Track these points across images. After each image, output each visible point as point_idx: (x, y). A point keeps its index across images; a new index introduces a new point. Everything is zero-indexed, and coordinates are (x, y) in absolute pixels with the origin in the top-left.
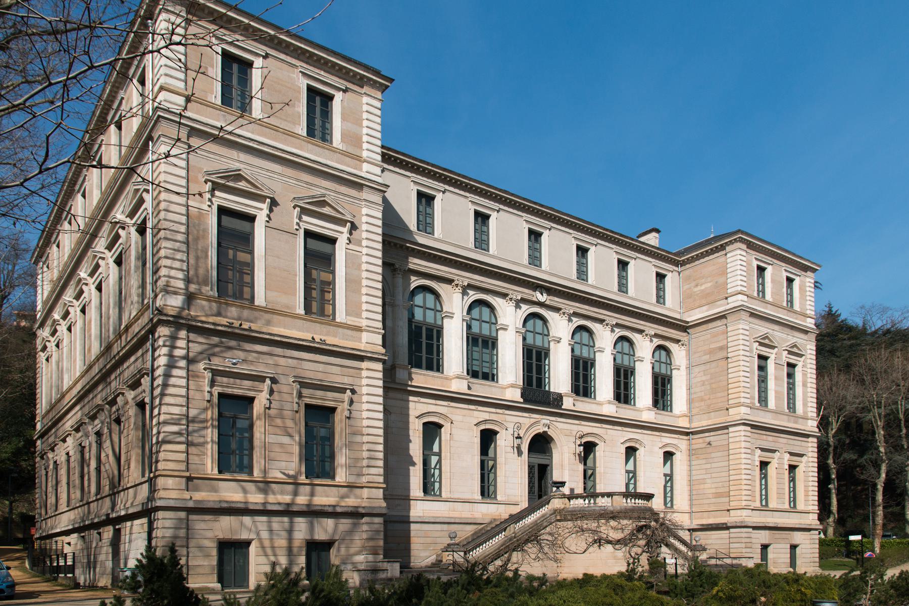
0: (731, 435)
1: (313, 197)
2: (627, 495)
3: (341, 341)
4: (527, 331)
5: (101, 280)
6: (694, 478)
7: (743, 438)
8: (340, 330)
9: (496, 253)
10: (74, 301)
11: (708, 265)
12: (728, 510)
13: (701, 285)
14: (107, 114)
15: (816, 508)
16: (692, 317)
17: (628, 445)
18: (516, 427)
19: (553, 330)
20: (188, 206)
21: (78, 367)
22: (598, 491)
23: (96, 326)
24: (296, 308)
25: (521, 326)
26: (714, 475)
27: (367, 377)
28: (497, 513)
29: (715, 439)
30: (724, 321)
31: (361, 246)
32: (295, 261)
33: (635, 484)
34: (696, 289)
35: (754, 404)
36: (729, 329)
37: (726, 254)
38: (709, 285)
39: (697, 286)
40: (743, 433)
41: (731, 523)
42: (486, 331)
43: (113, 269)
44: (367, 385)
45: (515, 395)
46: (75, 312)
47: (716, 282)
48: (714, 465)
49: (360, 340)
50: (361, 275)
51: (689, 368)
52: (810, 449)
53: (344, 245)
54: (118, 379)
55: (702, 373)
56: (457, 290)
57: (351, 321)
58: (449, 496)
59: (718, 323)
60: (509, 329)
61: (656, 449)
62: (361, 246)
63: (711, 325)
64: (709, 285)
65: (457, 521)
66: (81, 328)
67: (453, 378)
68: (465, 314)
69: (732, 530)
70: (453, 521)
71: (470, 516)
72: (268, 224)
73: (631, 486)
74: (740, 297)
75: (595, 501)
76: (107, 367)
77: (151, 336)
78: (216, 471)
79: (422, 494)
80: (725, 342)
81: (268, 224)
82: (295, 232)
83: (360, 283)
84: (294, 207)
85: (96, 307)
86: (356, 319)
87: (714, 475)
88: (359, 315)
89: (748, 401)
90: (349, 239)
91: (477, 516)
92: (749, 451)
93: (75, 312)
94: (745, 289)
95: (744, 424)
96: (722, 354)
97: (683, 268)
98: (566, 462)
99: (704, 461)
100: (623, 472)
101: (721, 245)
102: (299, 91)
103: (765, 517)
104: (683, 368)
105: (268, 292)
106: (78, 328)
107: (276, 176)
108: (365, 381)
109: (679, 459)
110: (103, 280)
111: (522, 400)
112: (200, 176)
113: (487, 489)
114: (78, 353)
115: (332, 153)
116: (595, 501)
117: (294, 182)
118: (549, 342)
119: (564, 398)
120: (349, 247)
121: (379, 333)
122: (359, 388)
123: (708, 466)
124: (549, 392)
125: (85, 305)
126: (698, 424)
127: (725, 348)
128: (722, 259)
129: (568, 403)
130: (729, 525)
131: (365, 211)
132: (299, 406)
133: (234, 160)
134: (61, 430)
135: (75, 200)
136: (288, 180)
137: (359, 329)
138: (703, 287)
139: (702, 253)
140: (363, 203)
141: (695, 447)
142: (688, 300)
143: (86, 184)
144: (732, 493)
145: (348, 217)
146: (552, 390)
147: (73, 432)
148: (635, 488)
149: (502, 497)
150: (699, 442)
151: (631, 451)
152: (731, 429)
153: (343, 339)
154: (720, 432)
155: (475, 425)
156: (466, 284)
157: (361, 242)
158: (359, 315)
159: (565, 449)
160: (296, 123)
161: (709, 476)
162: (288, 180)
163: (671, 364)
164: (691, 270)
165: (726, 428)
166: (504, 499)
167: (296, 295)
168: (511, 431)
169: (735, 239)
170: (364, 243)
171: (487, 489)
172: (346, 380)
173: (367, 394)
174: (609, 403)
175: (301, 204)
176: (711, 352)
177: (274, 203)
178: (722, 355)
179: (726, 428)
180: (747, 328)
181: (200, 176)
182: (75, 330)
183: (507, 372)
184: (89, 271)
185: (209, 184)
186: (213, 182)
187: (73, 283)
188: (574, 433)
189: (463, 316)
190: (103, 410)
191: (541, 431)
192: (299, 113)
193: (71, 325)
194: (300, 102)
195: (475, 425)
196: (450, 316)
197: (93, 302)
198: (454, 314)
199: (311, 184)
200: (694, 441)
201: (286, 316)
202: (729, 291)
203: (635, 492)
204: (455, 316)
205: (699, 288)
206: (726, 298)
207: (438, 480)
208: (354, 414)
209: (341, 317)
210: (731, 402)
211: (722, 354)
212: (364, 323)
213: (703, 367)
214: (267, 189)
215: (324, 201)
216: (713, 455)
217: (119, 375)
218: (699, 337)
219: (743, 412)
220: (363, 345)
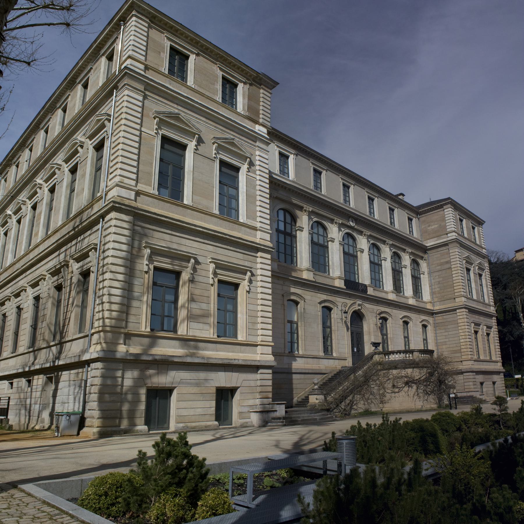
0: (458, 314)
1: (226, 139)
2: (405, 352)
3: (243, 235)
4: (345, 243)
5: (55, 183)
6: (439, 341)
7: (465, 316)
8: (243, 228)
9: (326, 194)
10: (27, 200)
11: (434, 216)
12: (461, 361)
13: (432, 226)
14: (77, 78)
15: (500, 359)
16: (429, 243)
17: (404, 320)
18: (343, 306)
19: (359, 244)
20: (141, 131)
21: (23, 247)
22: (390, 350)
23: (44, 218)
24: (213, 209)
25: (342, 240)
26: (450, 339)
27: (261, 263)
28: (334, 366)
29: (448, 317)
30: (447, 247)
31: (255, 174)
32: (213, 177)
33: (409, 345)
34: (429, 228)
35: (467, 296)
36: (451, 251)
37: (444, 210)
38: (436, 226)
39: (429, 226)
40: (465, 313)
41: (464, 369)
42: (321, 241)
43: (67, 177)
44: (261, 269)
45: (339, 284)
46: (27, 209)
47: (440, 225)
48: (450, 333)
49: (255, 236)
50: (256, 193)
51: (430, 273)
52: (494, 324)
53: (245, 173)
54: (81, 243)
55: (437, 277)
56: (305, 214)
57: (250, 222)
58: (305, 353)
59: (444, 248)
60: (335, 241)
61: (418, 323)
62: (255, 174)
63: (439, 249)
64: (436, 226)
65: (310, 371)
66: (30, 220)
67: (304, 270)
68: (310, 229)
69: (465, 374)
70: (307, 371)
71: (318, 368)
72: (195, 151)
73: (407, 347)
74: (454, 234)
75: (388, 357)
76: (70, 234)
77: (101, 220)
78: (216, 336)
79: (323, 354)
80: (449, 259)
81: (195, 151)
82: (214, 159)
83: (256, 198)
84: (213, 144)
85: (47, 204)
86: (253, 222)
87: (450, 339)
88: (255, 219)
89: (465, 294)
90: (248, 168)
91: (322, 368)
92: (468, 324)
93: (27, 209)
94: (456, 230)
95: (465, 308)
96: (447, 266)
97: (421, 216)
98: (372, 330)
99: (444, 331)
100: (403, 337)
101: (441, 205)
102: (217, 77)
103: (480, 365)
104: (426, 273)
105: (194, 197)
106: (26, 221)
107: (202, 122)
108: (259, 266)
109: (429, 328)
110: (57, 183)
111: (345, 288)
112: (151, 114)
113: (327, 349)
114: (25, 237)
115: (237, 115)
116: (388, 357)
117: (214, 128)
118: (357, 251)
119: (368, 288)
120: (248, 174)
121: (268, 233)
122: (255, 270)
123: (447, 334)
124: (358, 283)
125: (36, 203)
126: (437, 308)
127: (449, 262)
128: (442, 213)
129: (370, 291)
130: (463, 371)
131: (258, 153)
132: (214, 281)
133: (174, 109)
134: (86, 240)
135: (39, 134)
136: (209, 126)
137: (255, 229)
138: (433, 227)
139: (430, 209)
140: (257, 148)
141: (437, 322)
142: (423, 232)
143: (49, 123)
144: (462, 350)
145: (248, 155)
146: (360, 282)
147: (13, 297)
148: (409, 347)
149: (336, 354)
150: (439, 318)
151: (406, 323)
152: (458, 311)
153: (245, 235)
154: (451, 313)
155: (319, 303)
156: (311, 210)
157: (255, 172)
158: (255, 219)
159: (371, 321)
160: (217, 94)
161: (447, 340)
162: (209, 126)
163: (419, 271)
164: (425, 217)
165: (455, 310)
166: (338, 355)
167: (213, 200)
168: (340, 308)
169: (448, 202)
170: (258, 173)
171: (327, 349)
172: (246, 264)
173: (261, 275)
174: (392, 292)
175: (218, 141)
176: (442, 264)
177: (200, 141)
178: (447, 267)
179: (455, 310)
180: (460, 251)
181: (151, 114)
182: (25, 223)
183: (335, 269)
184: (45, 178)
185: (157, 119)
186: (160, 119)
187: (29, 187)
188: (375, 311)
189: (309, 230)
190: (44, 279)
191: (357, 309)
192: (217, 89)
193: (21, 218)
194: (218, 83)
195: (319, 303)
196: (301, 229)
197: (45, 202)
198: (303, 228)
199: (225, 131)
200: (436, 318)
201: (206, 214)
202: (448, 230)
203: (409, 350)
204: (304, 230)
205: (430, 228)
206: (447, 234)
207: (296, 342)
208: (253, 289)
209: (242, 219)
210: (456, 294)
211: (447, 266)
212: (258, 225)
213: (437, 274)
214: (196, 129)
215: (233, 142)
216: (449, 327)
217: (80, 241)
218: (433, 255)
219: (461, 301)
220: (258, 240)
